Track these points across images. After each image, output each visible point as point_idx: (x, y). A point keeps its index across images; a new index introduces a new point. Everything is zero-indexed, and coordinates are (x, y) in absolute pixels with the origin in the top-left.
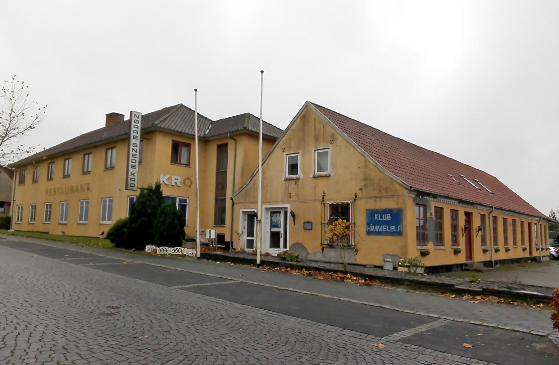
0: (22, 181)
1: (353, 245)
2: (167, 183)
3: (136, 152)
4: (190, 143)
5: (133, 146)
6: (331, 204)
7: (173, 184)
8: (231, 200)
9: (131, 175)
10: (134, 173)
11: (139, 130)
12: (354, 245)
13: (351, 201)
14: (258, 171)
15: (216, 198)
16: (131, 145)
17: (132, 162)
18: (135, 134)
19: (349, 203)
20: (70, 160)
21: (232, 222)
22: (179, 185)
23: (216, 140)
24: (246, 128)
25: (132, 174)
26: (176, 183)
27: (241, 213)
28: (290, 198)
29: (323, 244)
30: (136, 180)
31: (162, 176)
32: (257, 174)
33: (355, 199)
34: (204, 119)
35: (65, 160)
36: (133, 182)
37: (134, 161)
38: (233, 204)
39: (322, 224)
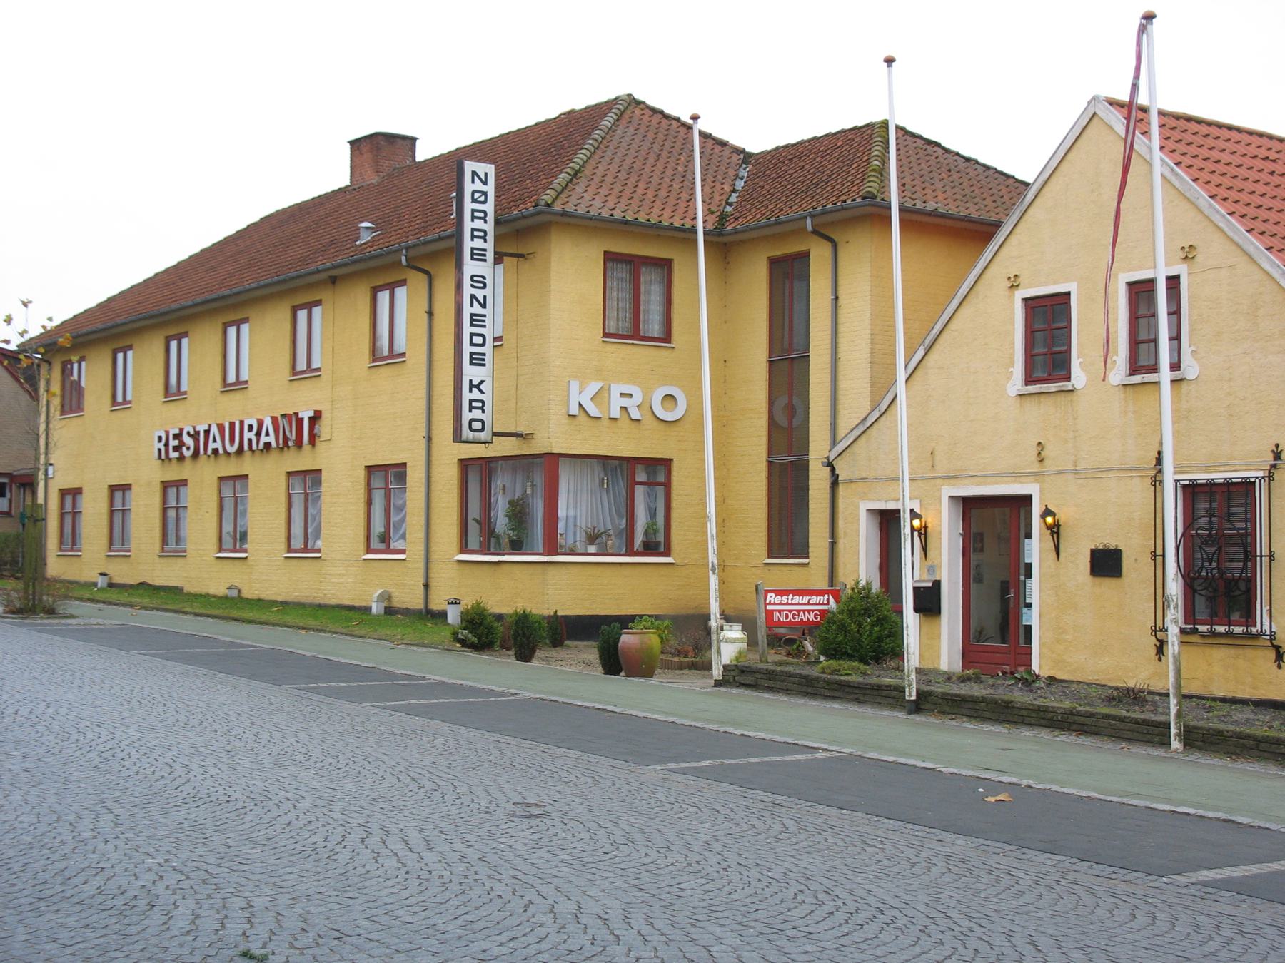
0: (73, 400)
1: (1264, 635)
2: (593, 410)
3: (473, 297)
4: (669, 257)
5: (472, 286)
6: (1187, 482)
7: (615, 413)
8: (828, 468)
9: (471, 391)
10: (482, 382)
11: (489, 227)
12: (1268, 633)
13: (1261, 474)
14: (896, 397)
15: (770, 459)
16: (467, 282)
17: (472, 344)
18: (478, 243)
19: (1252, 480)
20: (245, 328)
21: (833, 545)
22: (635, 414)
23: (766, 238)
24: (874, 197)
25: (475, 386)
26: (624, 409)
27: (863, 516)
28: (1042, 460)
29: (1161, 631)
30: (488, 408)
31: (575, 386)
32: (893, 407)
33: (1274, 466)
34: (718, 148)
35: (226, 326)
36: (477, 414)
37: (478, 340)
38: (835, 482)
39: (1154, 555)
